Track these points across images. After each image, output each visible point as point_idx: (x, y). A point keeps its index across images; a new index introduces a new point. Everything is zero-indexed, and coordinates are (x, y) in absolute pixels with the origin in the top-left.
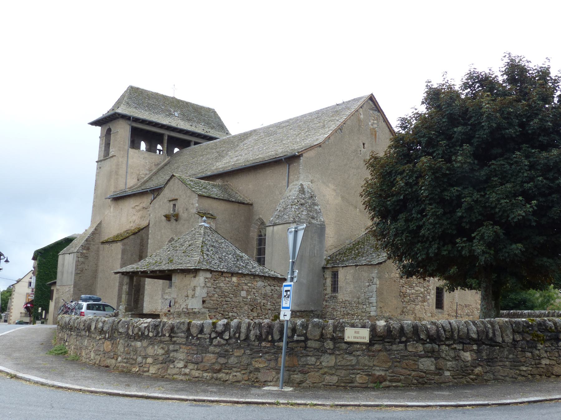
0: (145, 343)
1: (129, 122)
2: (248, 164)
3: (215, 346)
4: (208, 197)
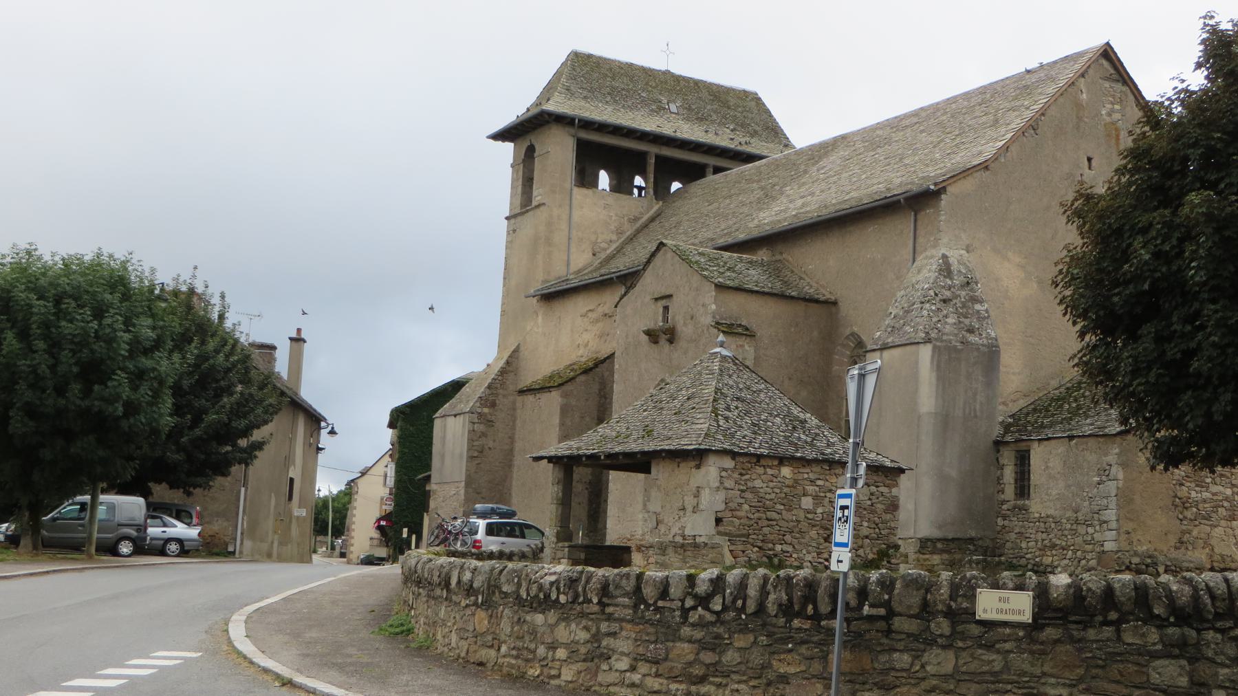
0: (552, 616)
1: (572, 131)
2: (826, 213)
3: (693, 625)
4: (738, 289)
